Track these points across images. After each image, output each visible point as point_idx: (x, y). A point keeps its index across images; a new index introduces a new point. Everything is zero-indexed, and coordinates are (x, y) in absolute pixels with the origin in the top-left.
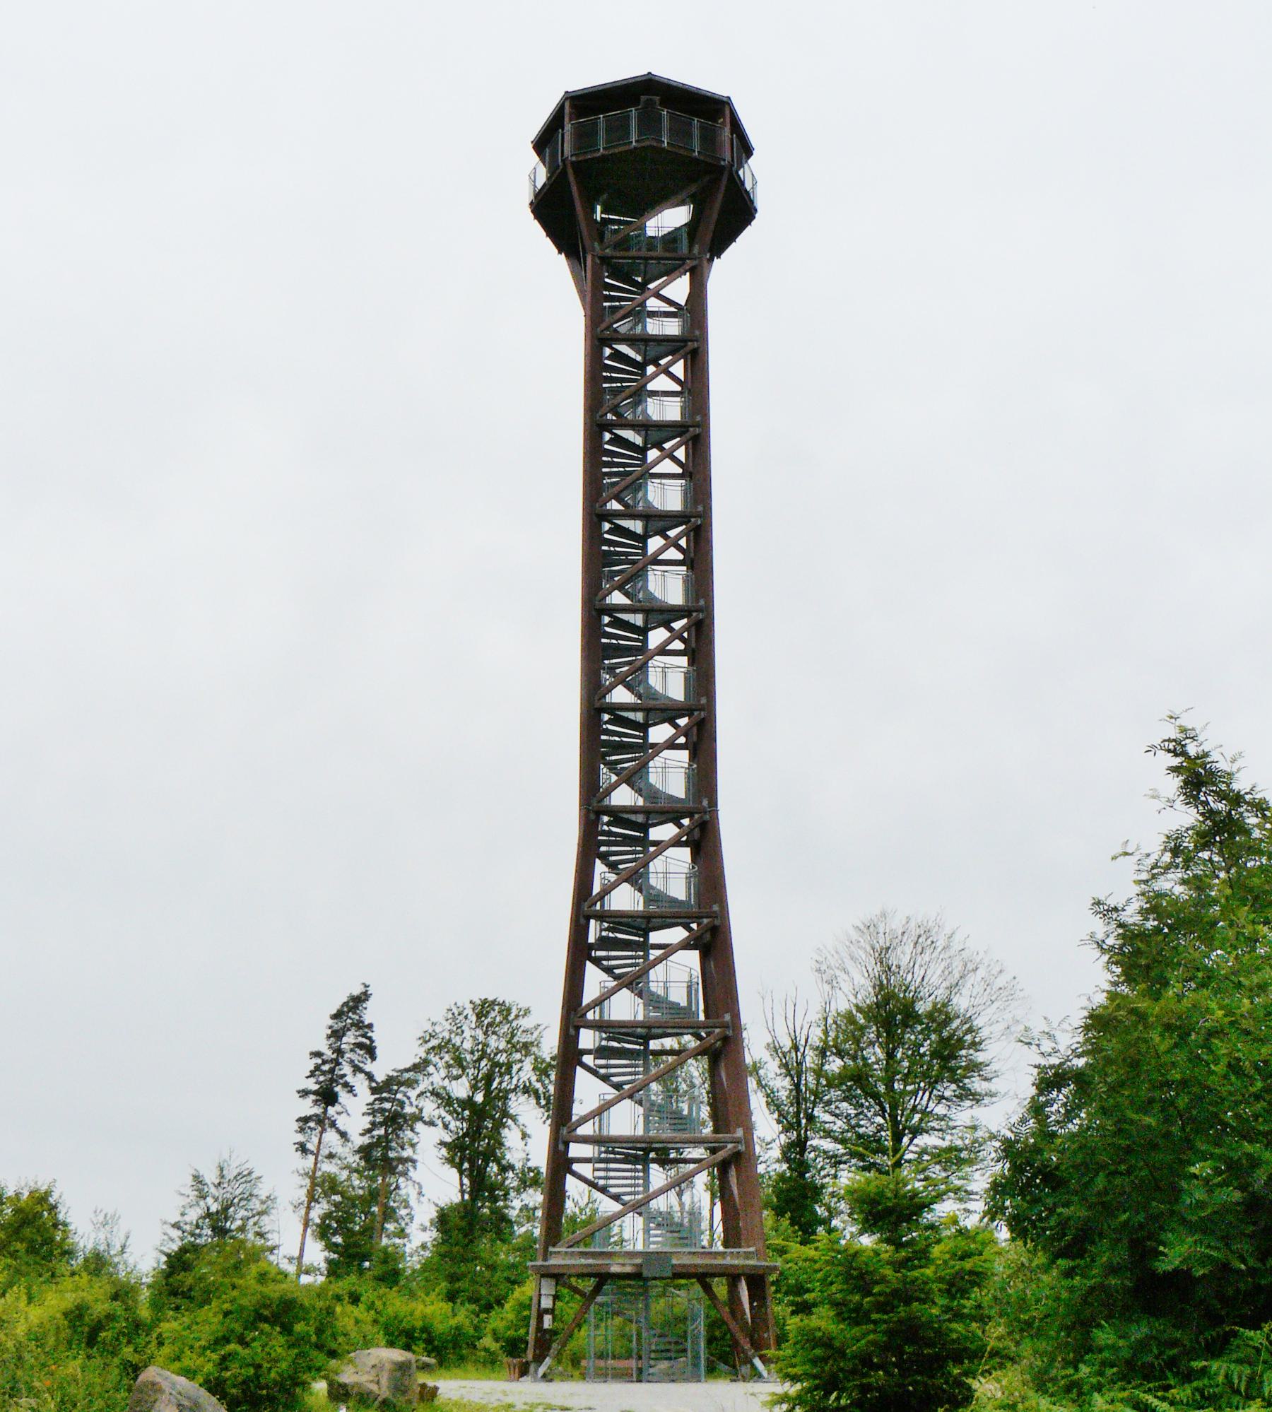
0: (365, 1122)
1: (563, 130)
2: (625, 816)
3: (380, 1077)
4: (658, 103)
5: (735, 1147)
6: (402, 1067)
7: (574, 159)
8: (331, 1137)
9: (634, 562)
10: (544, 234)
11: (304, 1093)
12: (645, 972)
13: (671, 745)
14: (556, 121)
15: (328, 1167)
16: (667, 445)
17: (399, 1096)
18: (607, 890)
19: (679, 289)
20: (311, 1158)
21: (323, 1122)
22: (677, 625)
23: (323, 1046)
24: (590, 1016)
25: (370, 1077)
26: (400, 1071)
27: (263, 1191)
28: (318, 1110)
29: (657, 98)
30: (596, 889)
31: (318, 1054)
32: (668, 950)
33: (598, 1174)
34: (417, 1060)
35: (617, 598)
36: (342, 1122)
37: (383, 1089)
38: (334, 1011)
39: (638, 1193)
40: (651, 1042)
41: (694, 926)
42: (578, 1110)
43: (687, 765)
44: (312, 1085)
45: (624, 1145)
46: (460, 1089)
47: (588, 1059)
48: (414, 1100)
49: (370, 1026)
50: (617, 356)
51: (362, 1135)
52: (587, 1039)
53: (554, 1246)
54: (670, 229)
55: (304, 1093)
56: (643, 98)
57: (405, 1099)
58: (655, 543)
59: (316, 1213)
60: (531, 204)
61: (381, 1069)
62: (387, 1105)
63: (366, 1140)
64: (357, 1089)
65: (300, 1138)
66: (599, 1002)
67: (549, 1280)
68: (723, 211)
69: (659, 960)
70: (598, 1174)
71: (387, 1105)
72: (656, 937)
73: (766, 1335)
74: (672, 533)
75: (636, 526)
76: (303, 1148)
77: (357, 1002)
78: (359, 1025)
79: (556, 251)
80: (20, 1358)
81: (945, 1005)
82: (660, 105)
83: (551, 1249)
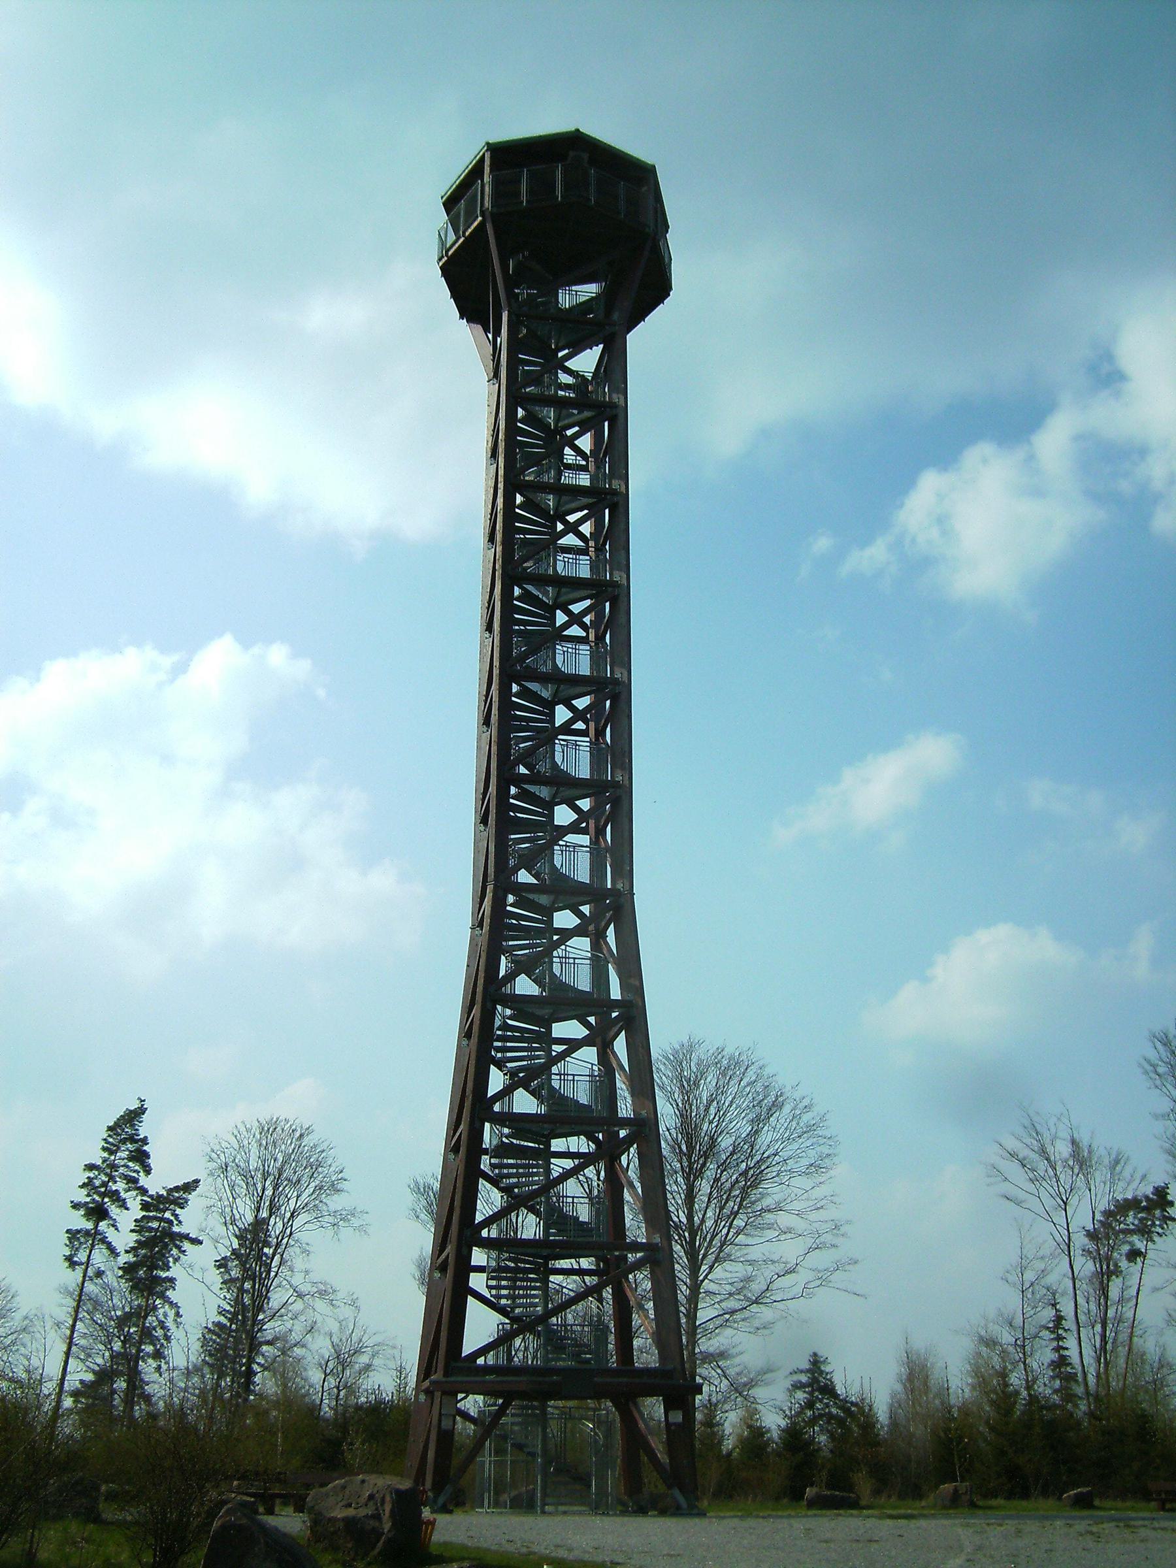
0: (131, 1239)
2: (531, 896)
7: (495, 210)
9: (538, 730)
11: (76, 1206)
12: (546, 1069)
13: (574, 828)
14: (476, 172)
16: (572, 518)
17: (168, 1215)
18: (511, 977)
19: (586, 361)
20: (79, 1270)
21: (96, 1237)
22: (582, 703)
24: (497, 1108)
25: (143, 1191)
28: (89, 1225)
29: (585, 156)
30: (502, 973)
32: (573, 1045)
35: (524, 877)
36: (111, 1235)
37: (155, 1204)
38: (111, 1124)
39: (538, 1057)
40: (554, 1142)
41: (592, 1019)
43: (589, 955)
44: (82, 1196)
45: (529, 1251)
48: (189, 1219)
49: (145, 1141)
50: (526, 597)
52: (489, 1135)
55: (76, 1206)
56: (572, 154)
57: (172, 1218)
58: (562, 714)
61: (155, 1184)
62: (155, 1225)
63: (131, 1258)
64: (129, 1203)
66: (499, 1096)
69: (562, 1056)
71: (155, 1225)
72: (561, 1029)
74: (576, 608)
75: (544, 792)
76: (71, 1262)
77: (133, 1116)
78: (132, 1139)
80: (830, 1145)
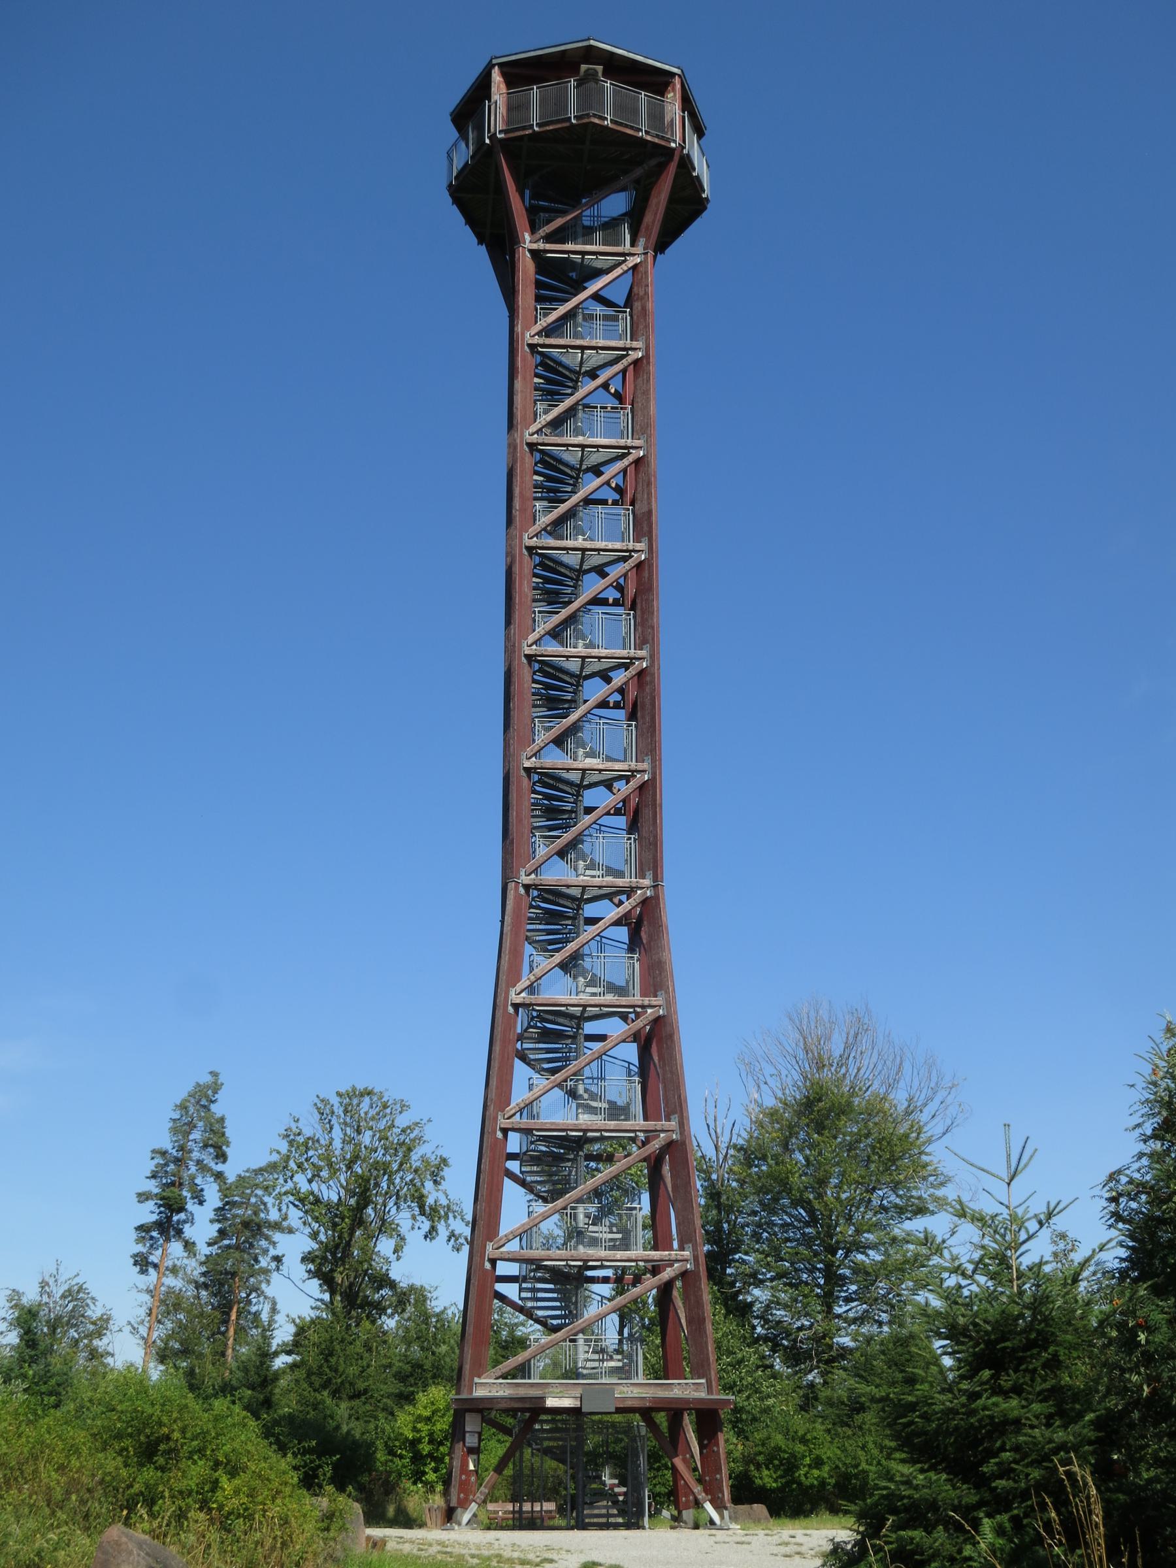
0: (213, 1230)
1: (490, 101)
3: (231, 1178)
4: (600, 74)
5: (681, 1266)
6: (255, 1166)
8: (176, 1248)
10: (463, 220)
11: (143, 1197)
15: (170, 1281)
23: (166, 1143)
25: (219, 1176)
26: (254, 1171)
27: (94, 1312)
29: (600, 68)
31: (163, 1153)
33: (524, 1295)
34: (275, 1157)
42: (505, 1228)
44: (153, 1187)
46: (331, 1194)
47: (514, 1166)
51: (209, 1244)
53: (479, 1377)
54: (606, 219)
55: (143, 1197)
56: (584, 67)
59: (159, 1333)
60: (450, 186)
61: (232, 1170)
63: (214, 1250)
65: (140, 1248)
67: (474, 1414)
68: (672, 200)
70: (524, 1295)
73: (718, 1476)
79: (475, 240)
81: (884, 1099)
82: (604, 76)
83: (476, 1380)
